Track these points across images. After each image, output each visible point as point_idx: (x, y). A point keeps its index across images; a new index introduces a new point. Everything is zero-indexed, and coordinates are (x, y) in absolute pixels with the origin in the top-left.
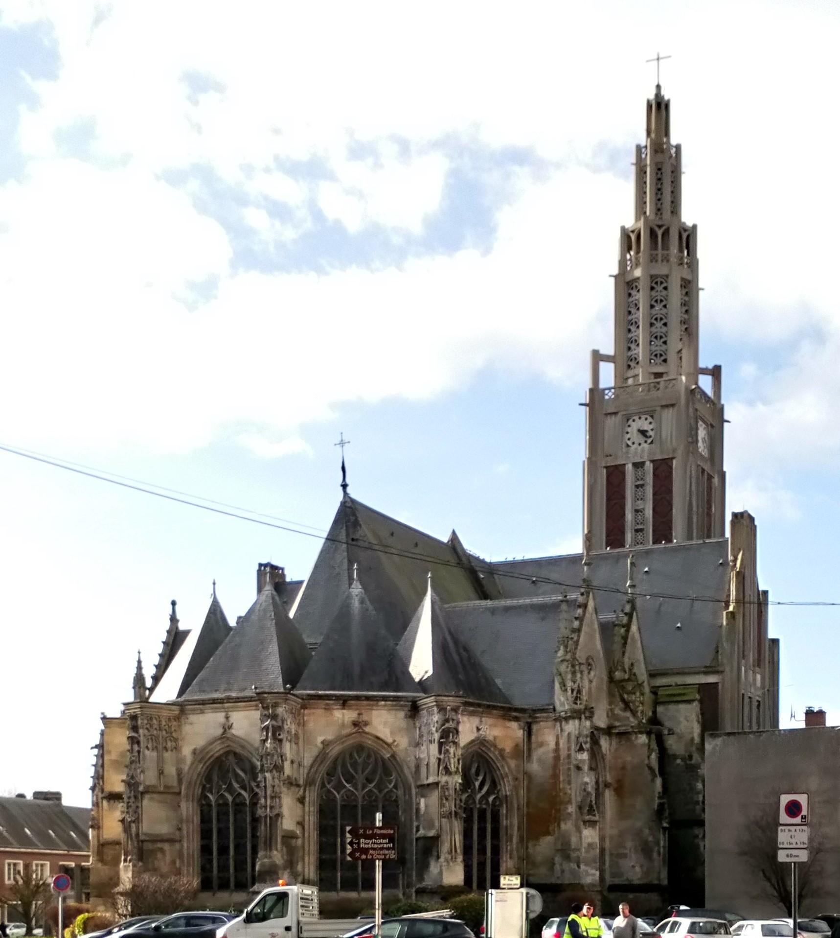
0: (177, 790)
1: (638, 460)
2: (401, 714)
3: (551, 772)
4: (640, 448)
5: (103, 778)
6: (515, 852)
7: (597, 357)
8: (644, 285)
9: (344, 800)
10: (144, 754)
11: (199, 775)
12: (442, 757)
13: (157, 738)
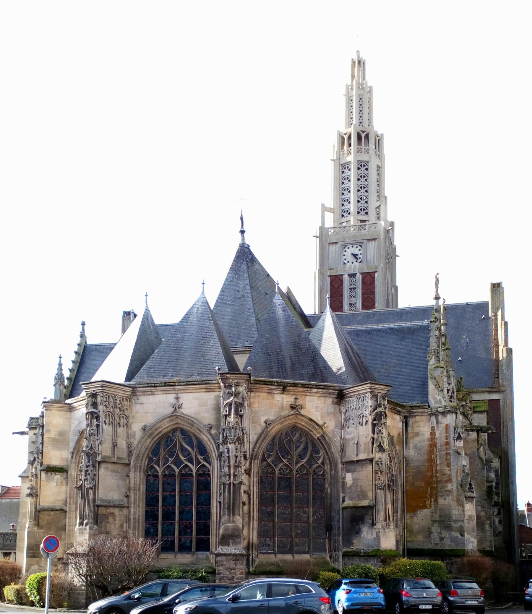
0: (127, 462)
1: (352, 272)
2: (330, 401)
3: (426, 457)
4: (353, 265)
5: (42, 453)
6: (399, 522)
7: (324, 209)
8: (353, 167)
9: (281, 474)
10: (102, 427)
11: (147, 448)
12: (375, 436)
13: (113, 415)
